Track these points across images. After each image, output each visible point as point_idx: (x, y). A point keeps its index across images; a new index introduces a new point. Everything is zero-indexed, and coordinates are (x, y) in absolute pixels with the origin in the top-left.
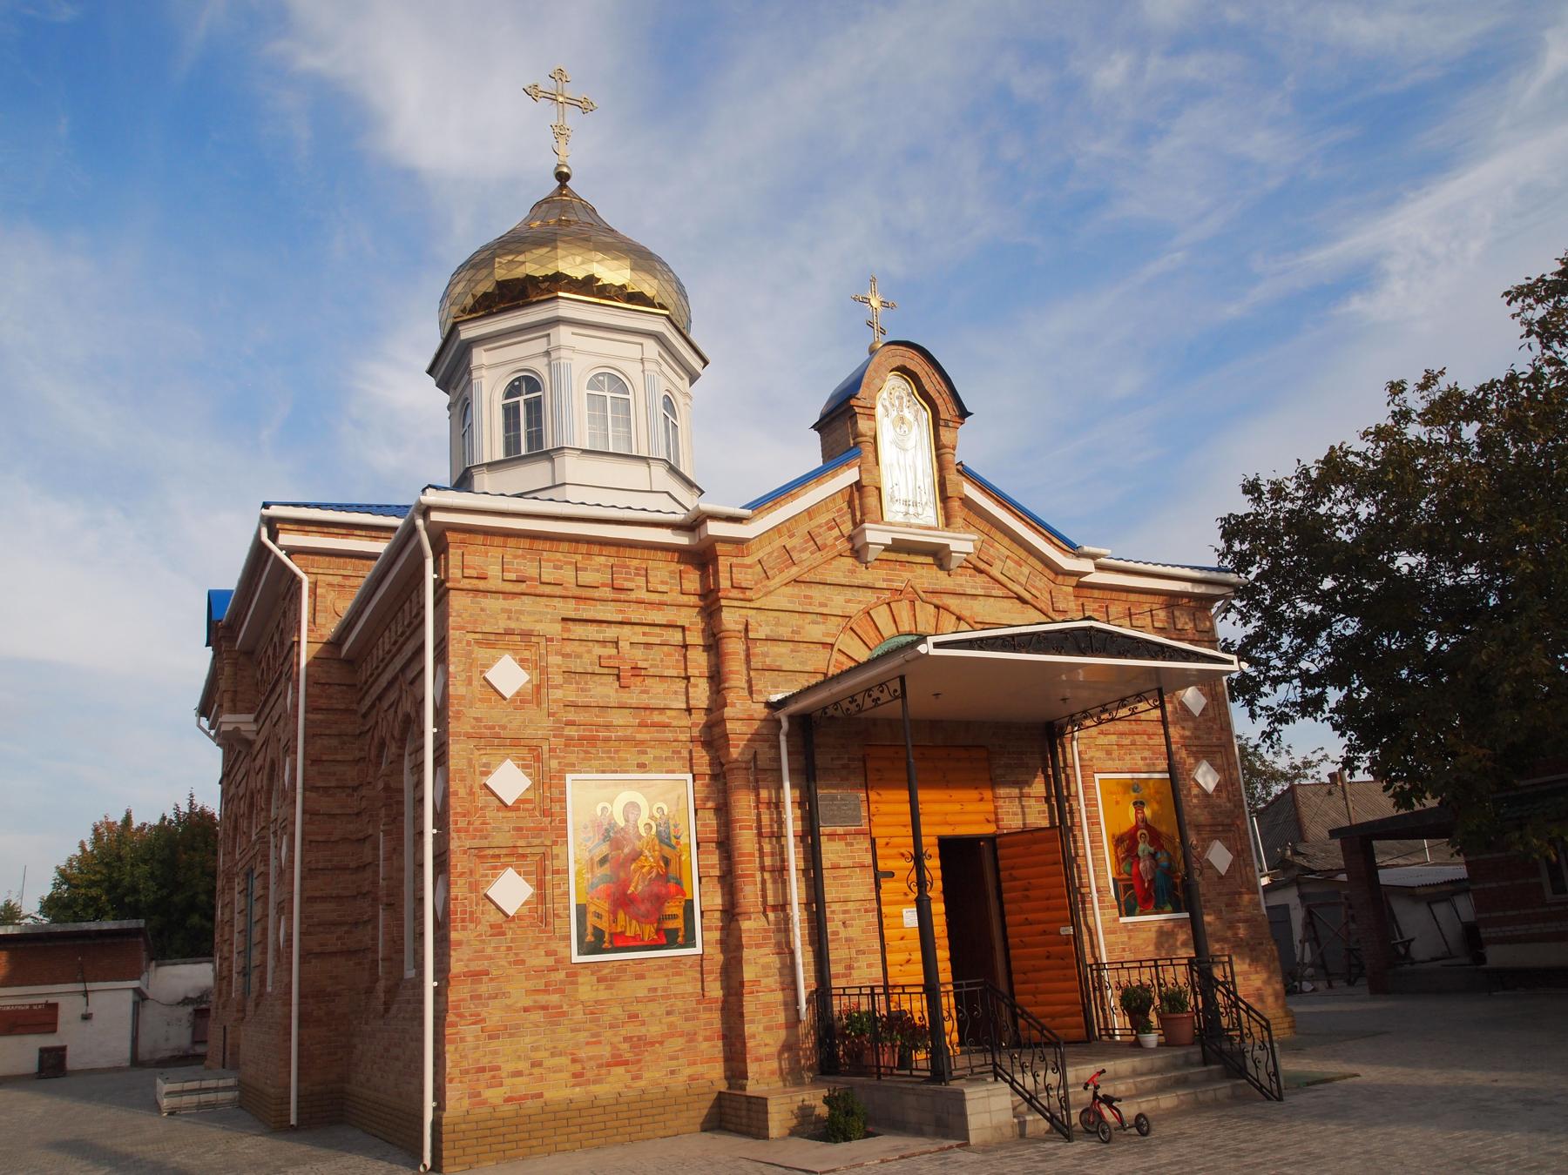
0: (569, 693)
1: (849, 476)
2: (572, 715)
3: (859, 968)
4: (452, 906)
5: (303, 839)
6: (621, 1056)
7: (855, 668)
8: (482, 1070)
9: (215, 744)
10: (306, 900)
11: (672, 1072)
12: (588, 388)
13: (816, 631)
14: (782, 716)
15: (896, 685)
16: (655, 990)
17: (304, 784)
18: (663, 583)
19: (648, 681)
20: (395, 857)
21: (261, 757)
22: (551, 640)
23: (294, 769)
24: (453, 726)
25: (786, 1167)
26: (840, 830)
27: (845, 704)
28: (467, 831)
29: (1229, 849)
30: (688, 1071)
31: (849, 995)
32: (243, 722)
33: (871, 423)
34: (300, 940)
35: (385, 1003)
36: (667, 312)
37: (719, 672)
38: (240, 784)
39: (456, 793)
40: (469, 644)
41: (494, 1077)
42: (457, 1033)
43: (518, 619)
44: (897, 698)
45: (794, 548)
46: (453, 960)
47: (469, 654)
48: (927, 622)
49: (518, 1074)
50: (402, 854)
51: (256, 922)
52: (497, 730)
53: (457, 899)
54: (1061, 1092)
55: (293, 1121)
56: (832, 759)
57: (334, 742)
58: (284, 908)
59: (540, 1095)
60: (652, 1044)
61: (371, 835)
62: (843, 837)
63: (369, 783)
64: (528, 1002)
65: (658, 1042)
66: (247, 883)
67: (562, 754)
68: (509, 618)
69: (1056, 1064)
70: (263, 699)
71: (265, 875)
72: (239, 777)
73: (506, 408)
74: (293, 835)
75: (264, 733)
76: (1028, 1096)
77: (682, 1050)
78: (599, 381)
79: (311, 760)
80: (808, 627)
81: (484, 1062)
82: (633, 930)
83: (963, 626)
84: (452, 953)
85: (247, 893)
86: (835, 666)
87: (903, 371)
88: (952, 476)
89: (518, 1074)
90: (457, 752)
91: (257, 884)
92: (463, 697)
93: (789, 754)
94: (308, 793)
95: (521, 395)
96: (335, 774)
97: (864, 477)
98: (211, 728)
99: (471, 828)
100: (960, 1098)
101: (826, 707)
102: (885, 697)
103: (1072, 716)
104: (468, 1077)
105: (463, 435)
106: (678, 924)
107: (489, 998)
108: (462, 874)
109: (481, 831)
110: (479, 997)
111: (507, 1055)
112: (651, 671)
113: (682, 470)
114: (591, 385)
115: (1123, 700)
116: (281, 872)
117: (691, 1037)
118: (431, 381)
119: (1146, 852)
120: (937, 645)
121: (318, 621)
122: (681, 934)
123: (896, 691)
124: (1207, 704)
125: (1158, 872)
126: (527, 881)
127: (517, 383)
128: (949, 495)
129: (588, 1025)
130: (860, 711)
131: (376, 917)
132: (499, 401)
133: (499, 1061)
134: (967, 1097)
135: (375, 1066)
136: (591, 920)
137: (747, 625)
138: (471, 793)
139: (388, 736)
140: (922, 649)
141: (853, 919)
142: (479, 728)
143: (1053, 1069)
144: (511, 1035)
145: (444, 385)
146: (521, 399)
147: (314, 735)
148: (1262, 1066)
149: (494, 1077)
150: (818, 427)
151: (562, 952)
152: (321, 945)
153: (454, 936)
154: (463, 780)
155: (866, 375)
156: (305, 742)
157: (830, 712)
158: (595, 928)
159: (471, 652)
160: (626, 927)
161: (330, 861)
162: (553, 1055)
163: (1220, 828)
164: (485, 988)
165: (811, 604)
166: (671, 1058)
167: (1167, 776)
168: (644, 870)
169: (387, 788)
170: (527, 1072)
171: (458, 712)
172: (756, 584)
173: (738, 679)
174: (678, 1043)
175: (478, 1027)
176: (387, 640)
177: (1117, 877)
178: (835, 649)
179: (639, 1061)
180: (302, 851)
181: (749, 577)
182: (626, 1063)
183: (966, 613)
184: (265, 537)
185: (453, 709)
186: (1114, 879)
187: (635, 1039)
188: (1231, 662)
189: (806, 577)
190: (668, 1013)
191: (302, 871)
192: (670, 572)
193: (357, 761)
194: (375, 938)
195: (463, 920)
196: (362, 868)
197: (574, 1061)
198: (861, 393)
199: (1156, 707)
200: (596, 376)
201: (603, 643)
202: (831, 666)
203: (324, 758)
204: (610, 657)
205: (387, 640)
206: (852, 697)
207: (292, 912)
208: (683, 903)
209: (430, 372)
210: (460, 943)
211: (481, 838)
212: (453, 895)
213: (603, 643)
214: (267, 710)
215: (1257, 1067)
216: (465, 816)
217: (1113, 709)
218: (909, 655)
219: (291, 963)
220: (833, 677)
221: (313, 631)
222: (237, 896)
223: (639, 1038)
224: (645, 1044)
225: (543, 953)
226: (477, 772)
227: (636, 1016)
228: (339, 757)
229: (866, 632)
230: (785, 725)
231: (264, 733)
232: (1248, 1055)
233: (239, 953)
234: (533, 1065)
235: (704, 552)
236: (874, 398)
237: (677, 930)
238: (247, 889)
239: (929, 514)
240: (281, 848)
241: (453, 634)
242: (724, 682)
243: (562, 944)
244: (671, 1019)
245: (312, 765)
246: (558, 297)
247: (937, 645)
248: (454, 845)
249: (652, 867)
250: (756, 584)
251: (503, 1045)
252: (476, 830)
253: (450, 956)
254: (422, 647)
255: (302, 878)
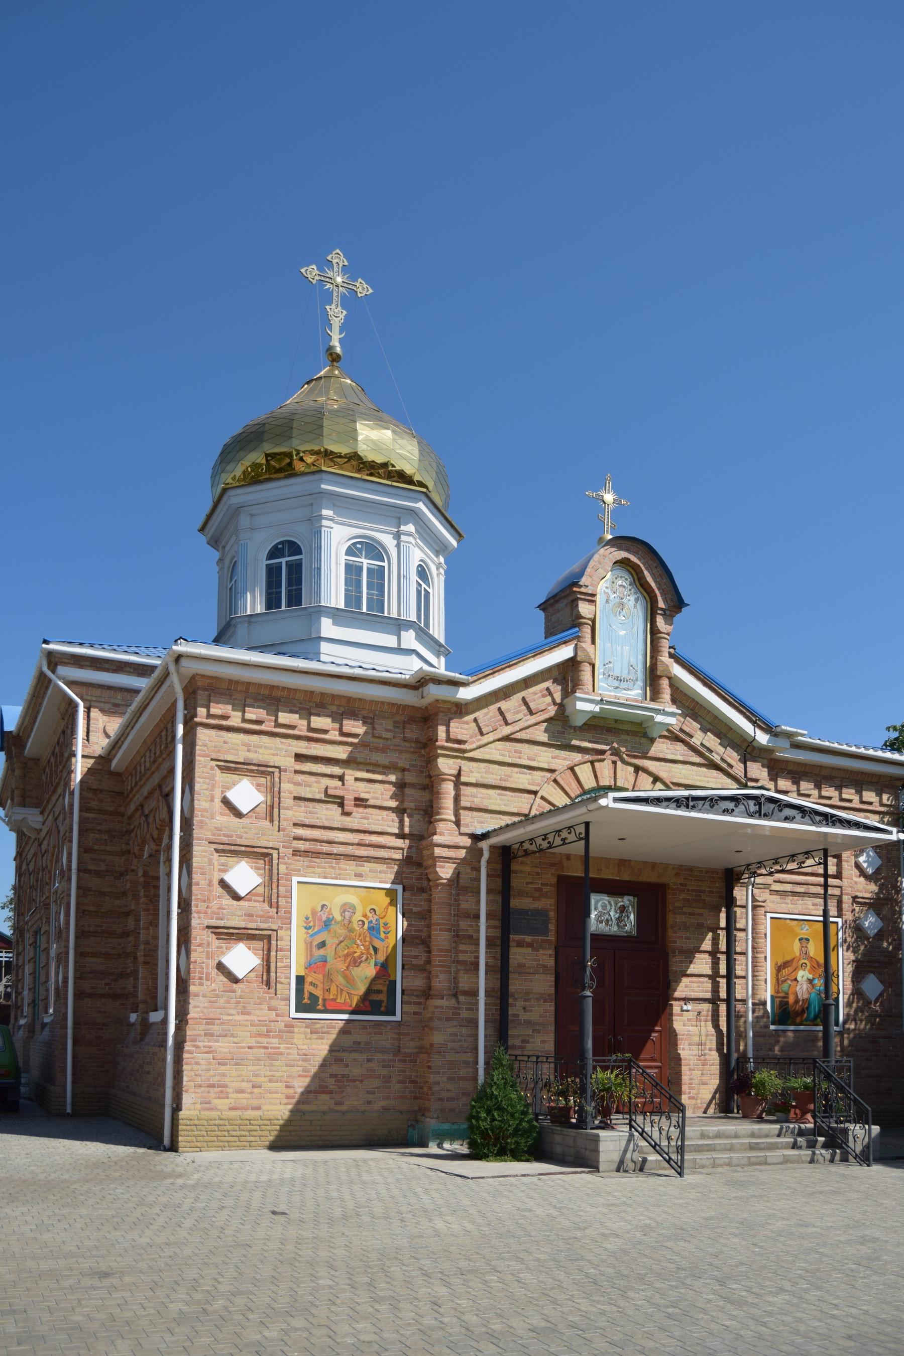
0: (299, 813)
1: (564, 653)
2: (300, 832)
3: (533, 1042)
4: (191, 967)
5: (77, 908)
6: (327, 1087)
7: (550, 811)
8: (213, 1086)
9: (7, 828)
10: (79, 954)
11: (369, 1102)
12: (347, 554)
13: (523, 779)
14: (484, 845)
15: (581, 829)
16: (359, 1043)
17: (78, 866)
18: (387, 730)
19: (369, 810)
20: (151, 928)
21: (45, 842)
22: (285, 771)
23: (70, 854)
24: (196, 832)
25: (446, 1173)
26: (528, 939)
27: (539, 841)
28: (206, 913)
29: (881, 982)
30: (383, 1103)
31: (520, 1061)
32: (33, 817)
33: (592, 608)
34: (75, 983)
35: (141, 1034)
36: (424, 490)
37: (432, 807)
38: (30, 861)
39: (197, 884)
40: (212, 769)
41: (222, 1092)
42: (193, 1058)
43: (256, 752)
44: (581, 839)
45: (509, 710)
46: (191, 1006)
47: (212, 778)
48: (627, 779)
49: (241, 1091)
50: (157, 926)
51: (42, 967)
52: (234, 838)
53: (196, 962)
54: (679, 1143)
55: (69, 1110)
56: (527, 883)
57: (105, 837)
58: (62, 959)
59: (258, 1108)
60: (354, 1081)
61: (133, 910)
62: (530, 945)
63: (133, 870)
64: (252, 1042)
65: (358, 1080)
66: (36, 938)
67: (290, 861)
68: (249, 751)
69: (678, 1122)
70: (47, 796)
71: (47, 932)
72: (29, 857)
73: (270, 568)
74: (68, 904)
75: (48, 823)
76: (653, 1143)
77: (377, 1088)
78: (357, 548)
79: (84, 849)
80: (515, 775)
81: (215, 1080)
82: (343, 998)
83: (659, 785)
84: (191, 1001)
85: (34, 945)
86: (539, 807)
87: (623, 563)
88: (665, 658)
89: (241, 1091)
90: (201, 853)
91: (43, 938)
92: (206, 810)
93: (488, 876)
94: (82, 874)
95: (283, 556)
96: (105, 860)
97: (579, 653)
98: (6, 816)
99: (209, 911)
100: (596, 1139)
101: (523, 842)
102: (572, 837)
103: (749, 865)
104: (199, 1090)
105: (231, 589)
106: (383, 997)
107: (220, 1036)
108: (200, 945)
109: (218, 914)
110: (212, 1035)
111: (232, 1076)
112: (371, 802)
113: (431, 632)
114: (350, 552)
115: (793, 856)
116: (59, 934)
117: (387, 1080)
118: (202, 539)
119: (805, 978)
120: (616, 800)
121: (91, 738)
122: (384, 1004)
123: (580, 834)
124: (881, 865)
125: (813, 995)
126: (255, 954)
127: (280, 546)
128: (658, 673)
129: (300, 1063)
130: (550, 847)
131: (135, 972)
132: (263, 563)
133: (227, 1080)
134: (601, 1139)
135: (133, 1078)
136: (308, 988)
137: (460, 771)
138: (210, 884)
139: (148, 836)
140: (603, 802)
141: (532, 1006)
142: (220, 835)
143: (675, 1126)
144: (237, 1064)
145: (214, 542)
146: (283, 561)
147: (87, 830)
148: (859, 1142)
149: (222, 1092)
150: (543, 607)
151: (281, 1005)
152: (92, 988)
153: (192, 989)
154: (203, 874)
155: (591, 563)
156: (80, 834)
157: (526, 846)
158: (311, 994)
159: (214, 776)
160: (337, 995)
161: (101, 926)
162: (270, 1081)
163: (876, 965)
164: (216, 1029)
165: (520, 758)
166: (368, 1093)
167: (821, 919)
168: (356, 955)
169: (145, 875)
170: (249, 1091)
171: (201, 822)
172: (471, 737)
173: (447, 814)
174: (377, 1082)
175: (211, 1056)
176: (148, 759)
177: (776, 995)
178: (539, 795)
179: (342, 1092)
180: (77, 917)
181: (465, 732)
182: (331, 1092)
183: (663, 774)
184: (45, 669)
185: (197, 819)
186: (772, 996)
187: (340, 1076)
188: (890, 833)
189: (518, 736)
190: (368, 1061)
191: (76, 932)
192: (395, 722)
193: (122, 853)
194: (135, 987)
195: (201, 978)
196: (126, 934)
197: (287, 1087)
198: (584, 581)
199: (820, 864)
200: (354, 544)
201: (332, 776)
202: (534, 808)
203: (96, 847)
204: (336, 788)
205: (148, 759)
206: (545, 835)
207: (67, 962)
208: (387, 982)
209: (202, 529)
210: (197, 995)
211: (217, 919)
212: (192, 959)
213: (332, 776)
214: (50, 806)
215: (855, 1141)
216: (204, 901)
217: (784, 863)
218: (592, 806)
219: (67, 999)
220: (535, 817)
221: (86, 747)
222: (27, 947)
223: (343, 1076)
224: (348, 1081)
225: (266, 1007)
226: (216, 869)
227: (342, 1060)
228: (109, 848)
229: (569, 784)
230: (486, 855)
231: (48, 823)
232: (850, 1133)
233: (29, 989)
234: (254, 1087)
235: (426, 707)
236: (596, 586)
237: (381, 1002)
238: (36, 942)
239: (634, 693)
240: (60, 913)
241: (199, 759)
242: (438, 814)
243: (283, 1003)
244: (370, 1065)
245: (85, 852)
246: (321, 471)
247: (616, 800)
248: (194, 922)
249: (362, 954)
250: (471, 737)
251: (230, 1071)
252: (214, 913)
253: (189, 1003)
254: (172, 770)
255: (77, 937)
